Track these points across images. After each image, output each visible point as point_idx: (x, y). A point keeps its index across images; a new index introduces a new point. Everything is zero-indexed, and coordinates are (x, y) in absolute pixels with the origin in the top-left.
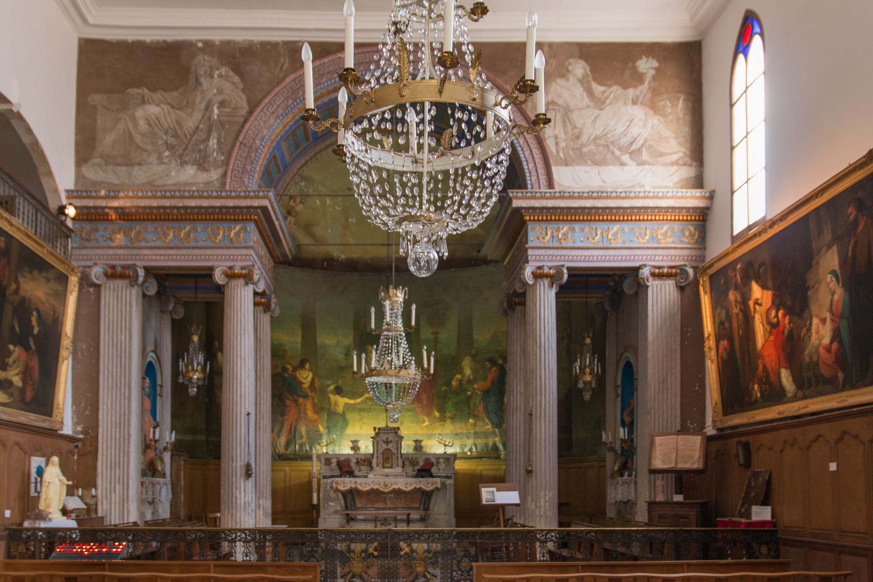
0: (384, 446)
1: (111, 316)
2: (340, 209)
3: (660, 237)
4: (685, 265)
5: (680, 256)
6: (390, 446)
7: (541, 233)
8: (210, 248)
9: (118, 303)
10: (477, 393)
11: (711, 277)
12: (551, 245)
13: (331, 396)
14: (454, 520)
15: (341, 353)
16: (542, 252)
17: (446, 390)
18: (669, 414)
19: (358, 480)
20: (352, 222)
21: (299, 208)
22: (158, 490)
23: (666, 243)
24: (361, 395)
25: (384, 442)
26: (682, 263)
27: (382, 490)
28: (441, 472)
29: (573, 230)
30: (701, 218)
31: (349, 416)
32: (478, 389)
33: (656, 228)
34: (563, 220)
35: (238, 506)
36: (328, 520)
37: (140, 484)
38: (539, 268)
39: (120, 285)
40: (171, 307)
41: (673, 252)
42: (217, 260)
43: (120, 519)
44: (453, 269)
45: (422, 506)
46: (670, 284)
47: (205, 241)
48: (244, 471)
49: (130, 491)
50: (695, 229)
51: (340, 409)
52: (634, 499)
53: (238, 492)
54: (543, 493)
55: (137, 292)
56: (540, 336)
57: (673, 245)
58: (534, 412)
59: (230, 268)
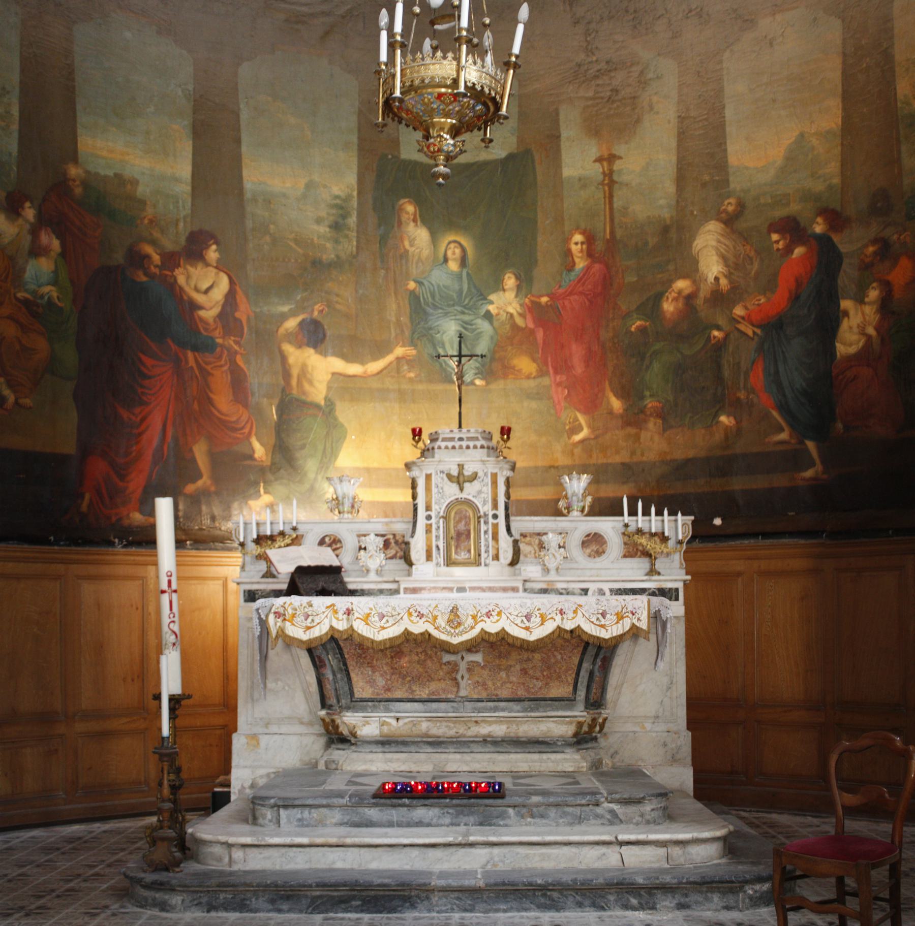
0: (452, 491)
6: (470, 491)
13: (289, 349)
15: (319, 221)
17: (642, 330)
24: (380, 350)
25: (450, 477)
27: (443, 637)
28: (372, 576)
31: (345, 413)
32: (747, 319)
36: (264, 740)
45: (581, 693)
51: (318, 392)
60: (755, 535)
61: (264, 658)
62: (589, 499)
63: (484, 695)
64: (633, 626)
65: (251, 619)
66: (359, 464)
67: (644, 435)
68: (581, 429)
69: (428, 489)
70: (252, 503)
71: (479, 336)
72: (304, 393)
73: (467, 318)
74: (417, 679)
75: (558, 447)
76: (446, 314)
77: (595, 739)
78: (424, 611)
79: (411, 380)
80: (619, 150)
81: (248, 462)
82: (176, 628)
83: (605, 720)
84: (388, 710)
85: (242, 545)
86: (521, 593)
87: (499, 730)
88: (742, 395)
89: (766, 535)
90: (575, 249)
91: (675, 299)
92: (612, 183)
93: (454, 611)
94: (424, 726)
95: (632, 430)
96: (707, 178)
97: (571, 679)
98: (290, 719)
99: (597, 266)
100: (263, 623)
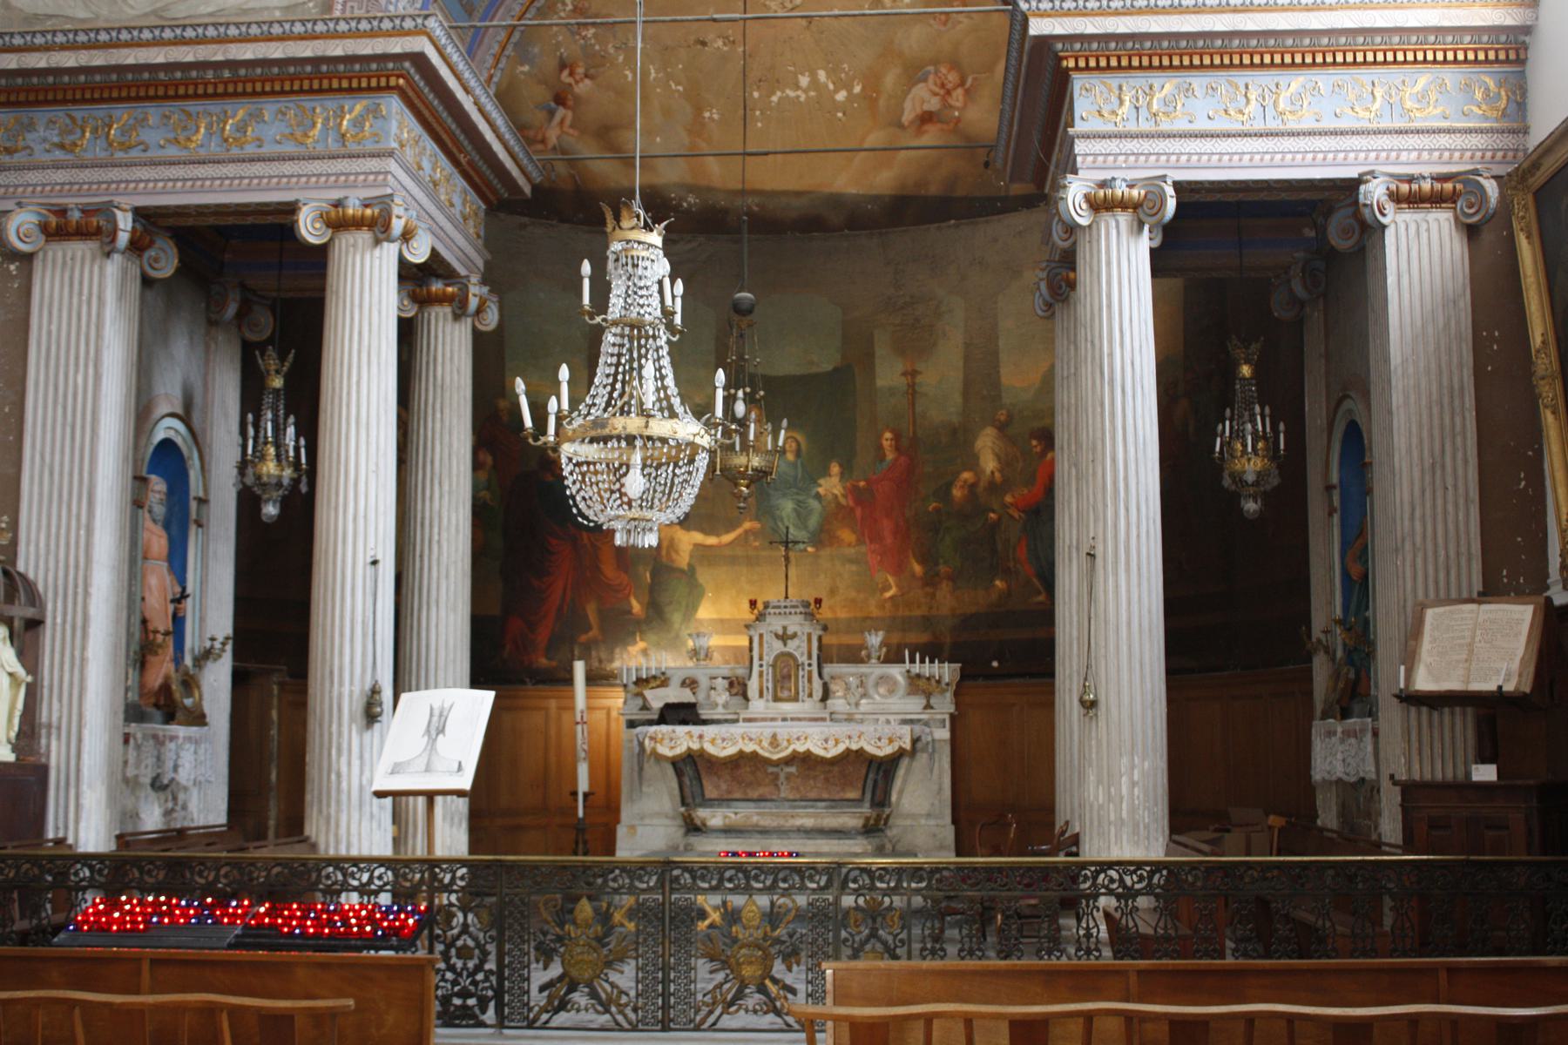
0: (778, 646)
1: (54, 328)
2: (680, 88)
3: (1409, 104)
4: (1476, 172)
5: (1463, 150)
6: (792, 646)
7: (1107, 101)
8: (291, 159)
9: (71, 297)
10: (1012, 517)
11: (1538, 194)
12: (1132, 127)
14: (949, 833)
16: (1112, 146)
17: (937, 510)
18: (1452, 554)
19: (709, 731)
20: (711, 118)
21: (584, 87)
22: (172, 755)
23: (1425, 119)
24: (731, 527)
25: (777, 636)
26: (1470, 167)
27: (766, 755)
28: (720, 709)
29: (1189, 91)
30: (1512, 56)
31: (704, 576)
33: (1398, 82)
34: (1161, 67)
35: (344, 797)
36: (640, 830)
37: (121, 740)
38: (1103, 184)
39: (79, 254)
40: (231, 310)
41: (1444, 141)
42: (306, 188)
43: (57, 828)
44: (953, 222)
45: (868, 796)
46: (1440, 221)
47: (279, 143)
48: (359, 706)
49: (85, 757)
50: (1500, 85)
51: (683, 560)
52: (1373, 776)
53: (344, 760)
54: (1125, 760)
55: (124, 272)
56: (1111, 355)
57: (1445, 124)
58: (1099, 552)
59: (338, 204)
60: (1022, 675)
61: (641, 769)
62: (884, 650)
63: (798, 796)
64: (900, 748)
65: (631, 741)
66: (715, 616)
67: (939, 594)
68: (890, 588)
69: (761, 644)
70: (630, 649)
71: (810, 512)
72: (672, 561)
73: (801, 498)
74: (750, 785)
75: (873, 602)
76: (784, 495)
77: (882, 831)
78: (753, 736)
79: (756, 548)
80: (920, 366)
81: (627, 617)
82: (586, 747)
83: (888, 816)
84: (729, 807)
85: (625, 686)
86: (828, 723)
87: (809, 822)
88: (1011, 564)
89: (1032, 675)
90: (886, 444)
91: (962, 487)
92: (914, 393)
93: (774, 736)
94: (755, 819)
95: (928, 589)
96: (985, 392)
97: (860, 785)
98: (658, 815)
99: (903, 459)
100: (641, 744)
